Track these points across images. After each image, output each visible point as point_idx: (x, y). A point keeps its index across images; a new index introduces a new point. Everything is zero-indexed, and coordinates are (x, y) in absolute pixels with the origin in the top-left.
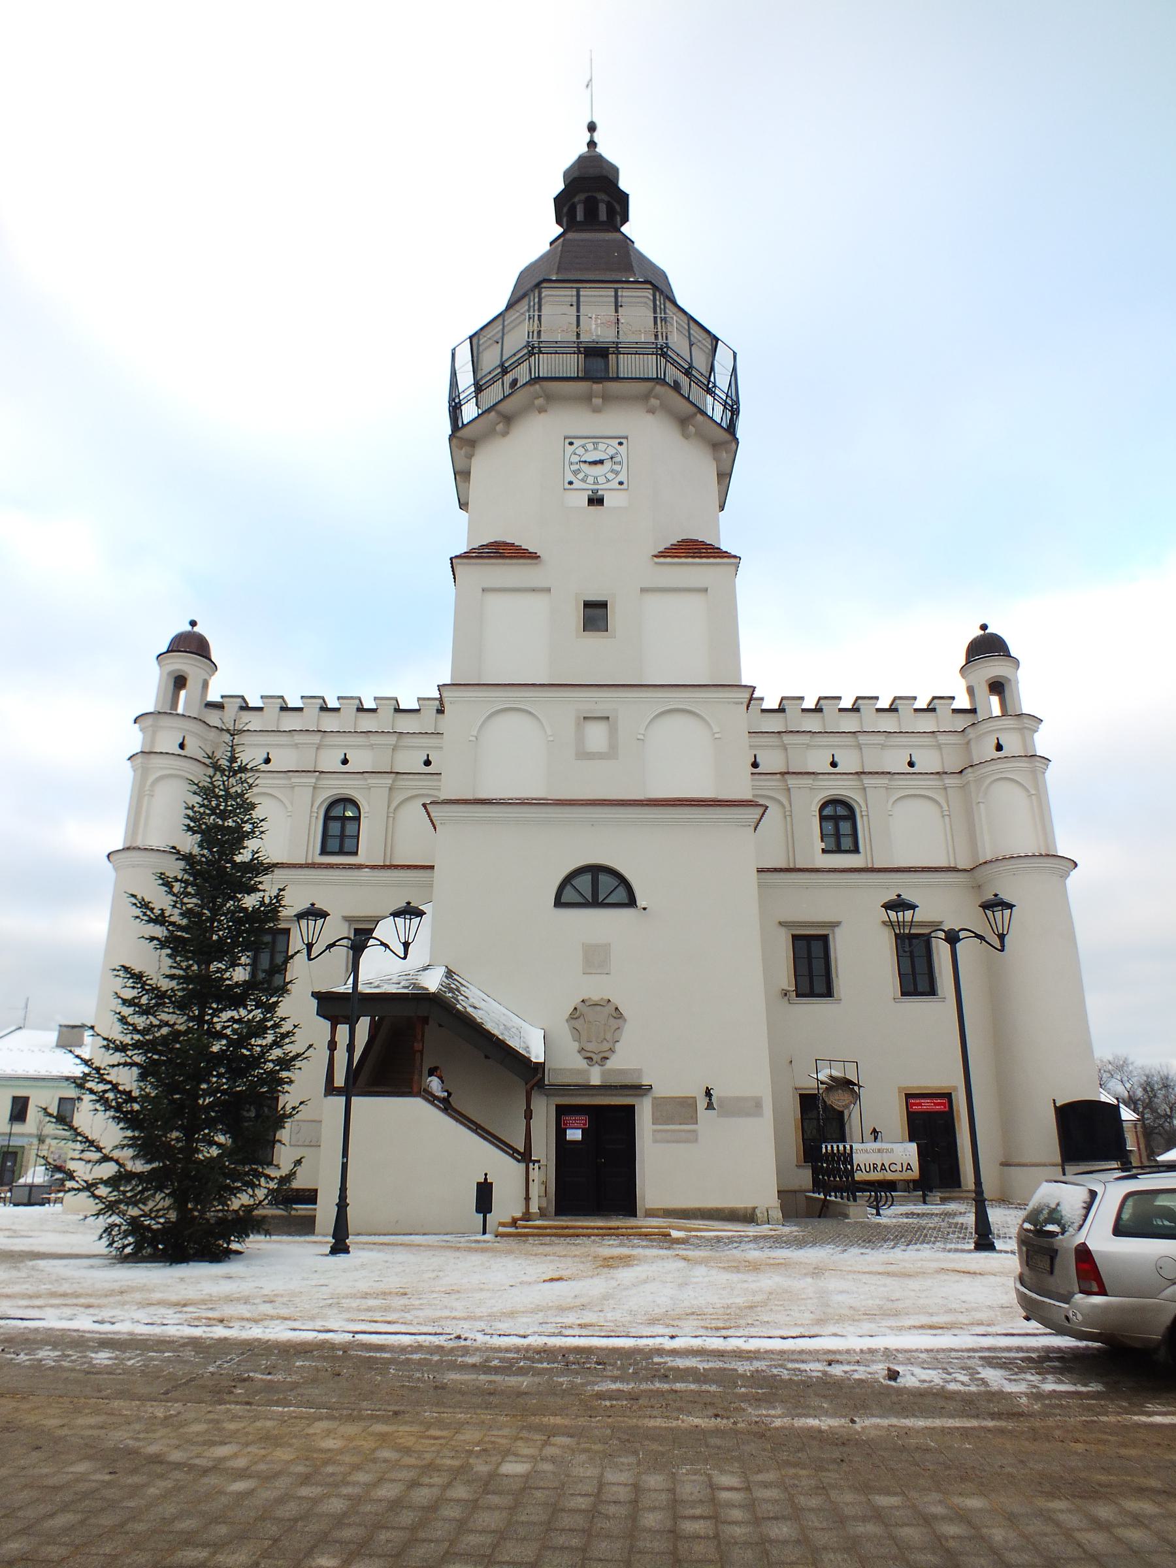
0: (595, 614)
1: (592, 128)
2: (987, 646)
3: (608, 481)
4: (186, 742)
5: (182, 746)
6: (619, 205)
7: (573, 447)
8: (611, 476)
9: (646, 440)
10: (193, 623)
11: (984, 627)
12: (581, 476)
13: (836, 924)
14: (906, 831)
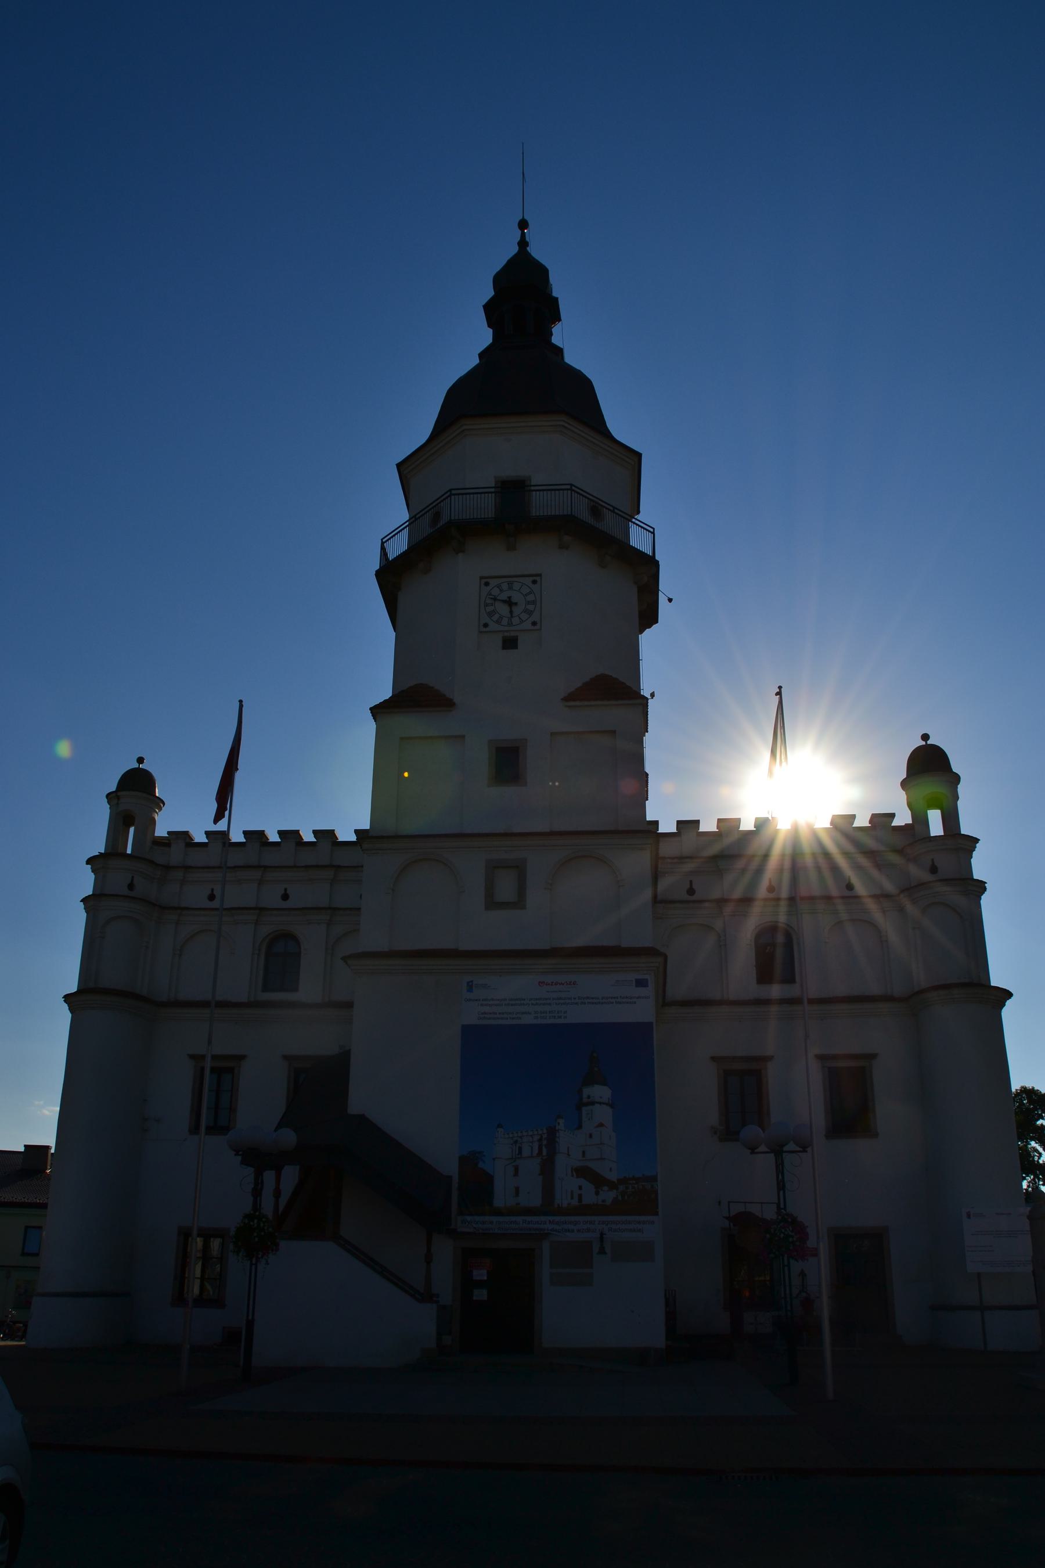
0: (591, 1136)
1: (523, 224)
3: (522, 621)
5: (131, 886)
6: (551, 311)
7: (489, 588)
8: (524, 616)
9: (559, 570)
10: (140, 760)
11: (925, 737)
12: (496, 617)
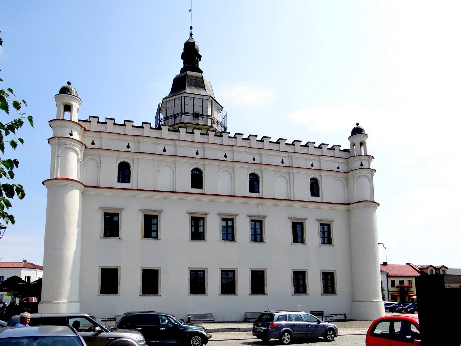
2: (357, 131)
4: (362, 163)
11: (357, 124)
13: (207, 214)
14: (330, 189)
